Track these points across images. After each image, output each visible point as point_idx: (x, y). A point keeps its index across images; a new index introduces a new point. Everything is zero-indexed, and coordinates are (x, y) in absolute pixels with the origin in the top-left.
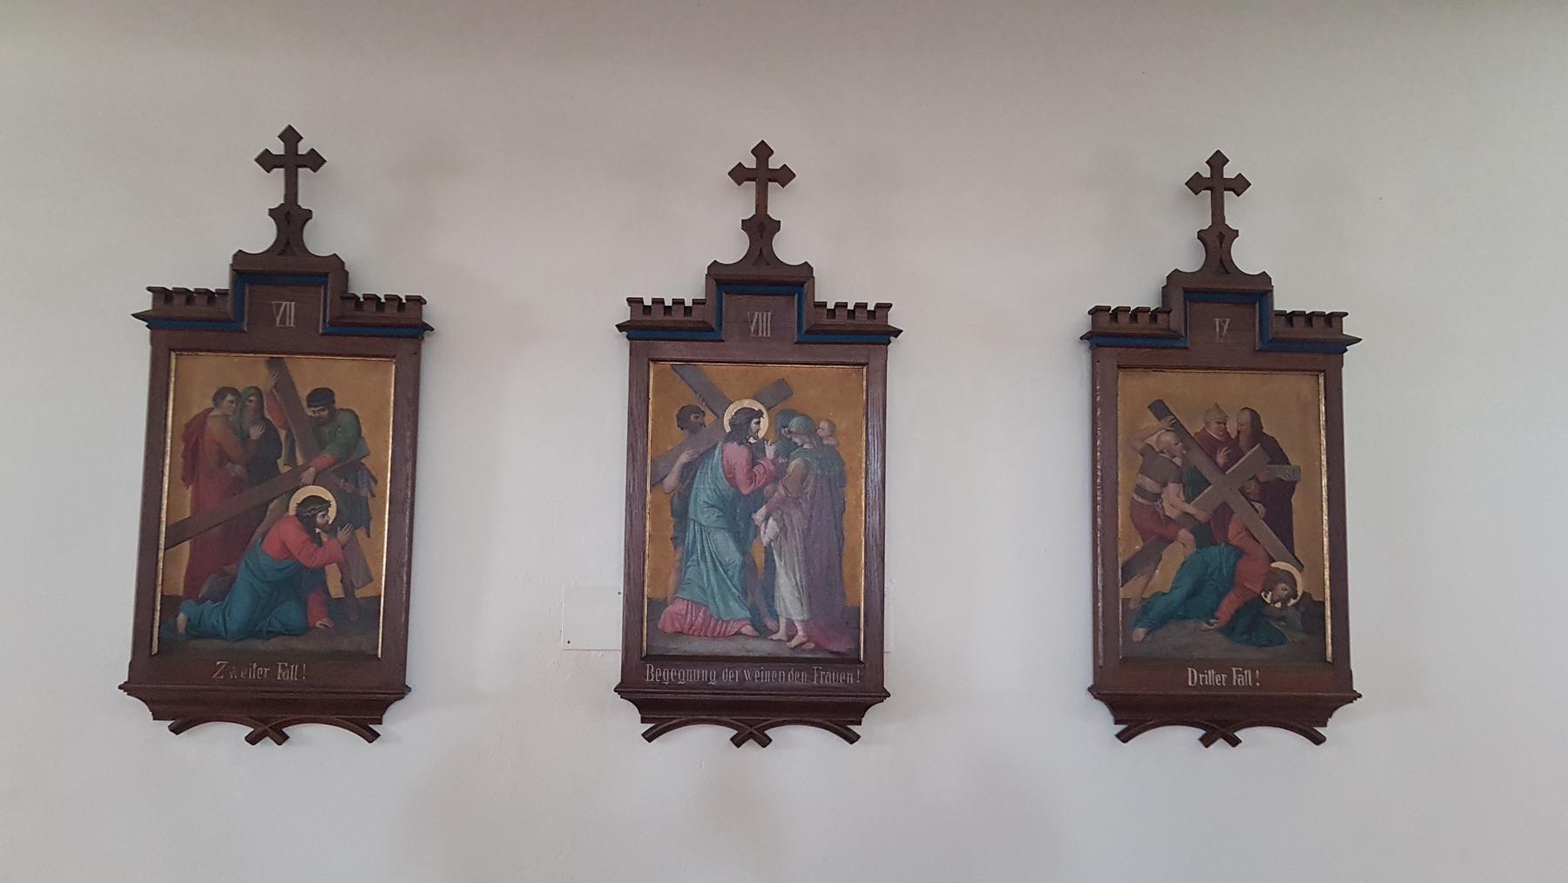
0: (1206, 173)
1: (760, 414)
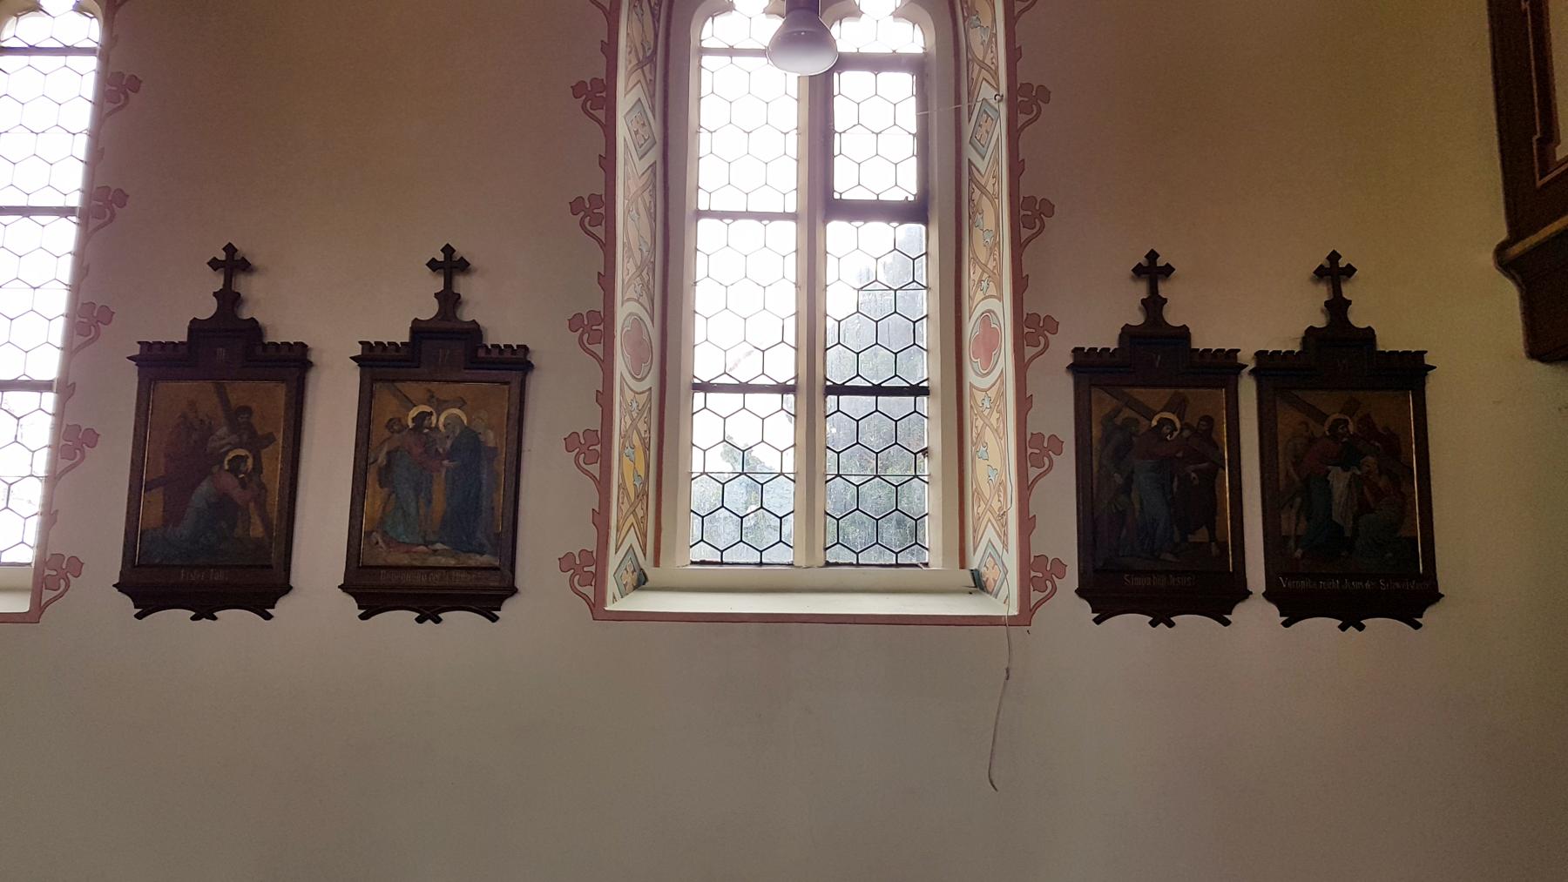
0: (1327, 265)
1: (431, 414)
